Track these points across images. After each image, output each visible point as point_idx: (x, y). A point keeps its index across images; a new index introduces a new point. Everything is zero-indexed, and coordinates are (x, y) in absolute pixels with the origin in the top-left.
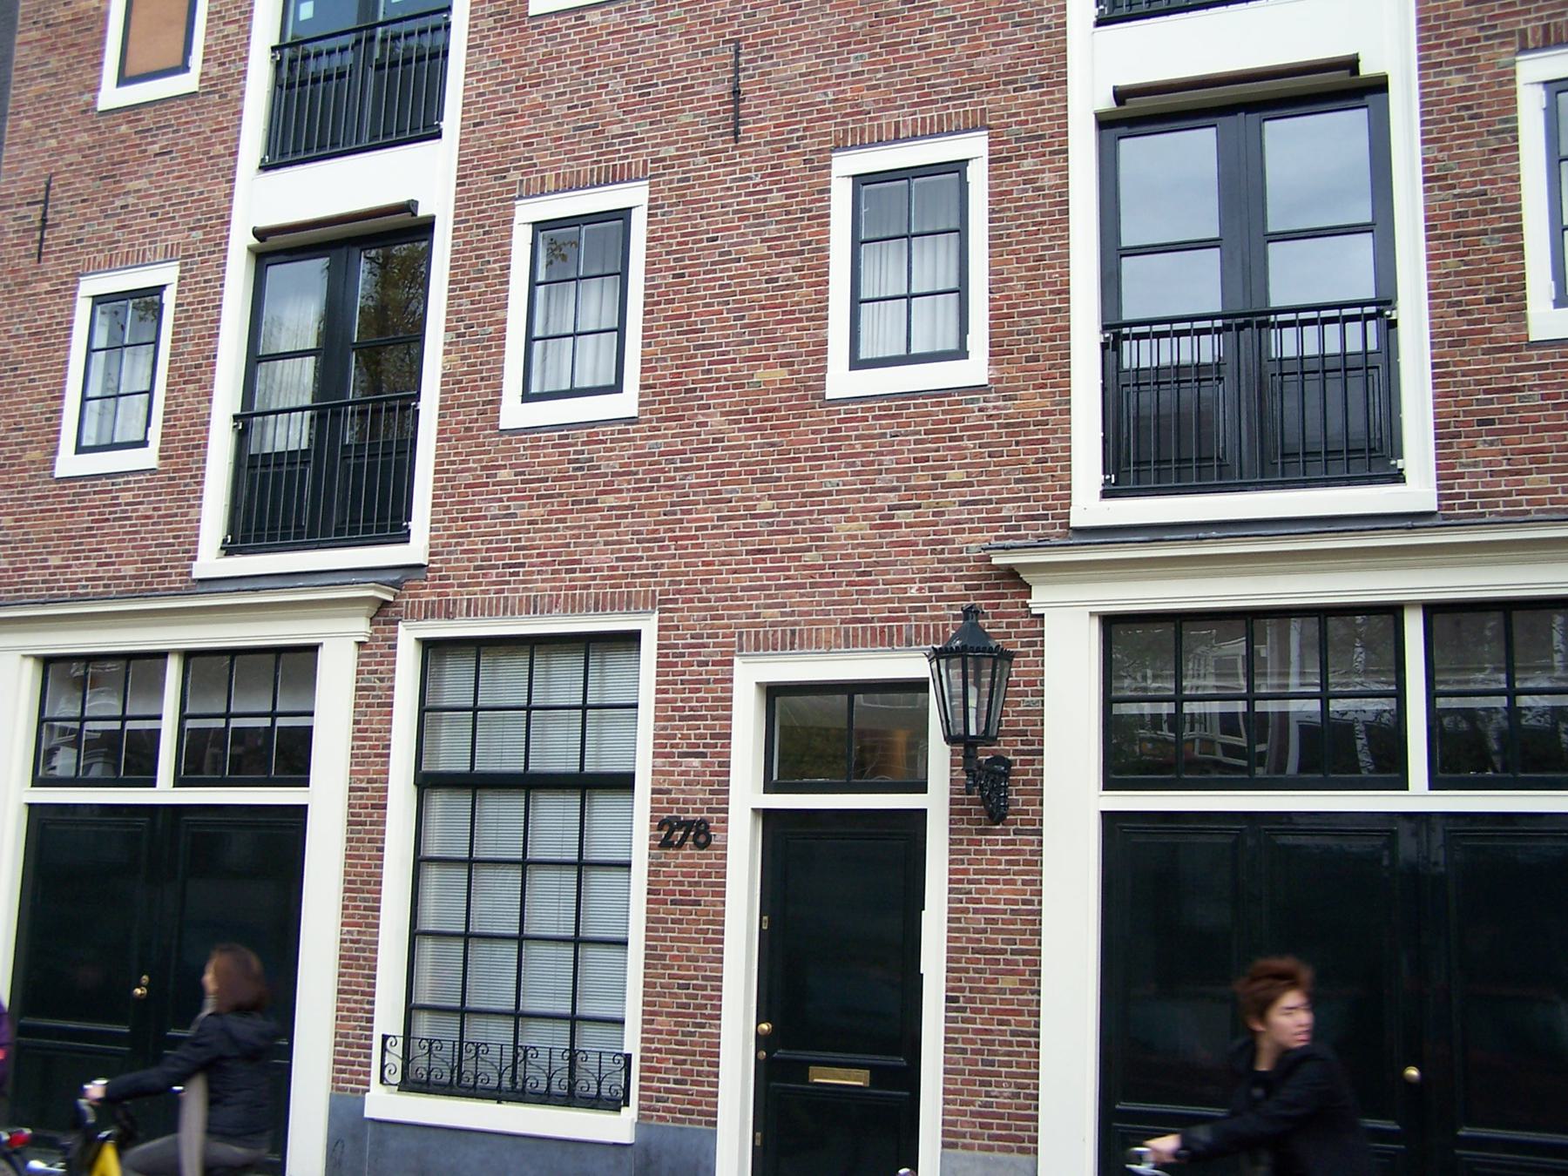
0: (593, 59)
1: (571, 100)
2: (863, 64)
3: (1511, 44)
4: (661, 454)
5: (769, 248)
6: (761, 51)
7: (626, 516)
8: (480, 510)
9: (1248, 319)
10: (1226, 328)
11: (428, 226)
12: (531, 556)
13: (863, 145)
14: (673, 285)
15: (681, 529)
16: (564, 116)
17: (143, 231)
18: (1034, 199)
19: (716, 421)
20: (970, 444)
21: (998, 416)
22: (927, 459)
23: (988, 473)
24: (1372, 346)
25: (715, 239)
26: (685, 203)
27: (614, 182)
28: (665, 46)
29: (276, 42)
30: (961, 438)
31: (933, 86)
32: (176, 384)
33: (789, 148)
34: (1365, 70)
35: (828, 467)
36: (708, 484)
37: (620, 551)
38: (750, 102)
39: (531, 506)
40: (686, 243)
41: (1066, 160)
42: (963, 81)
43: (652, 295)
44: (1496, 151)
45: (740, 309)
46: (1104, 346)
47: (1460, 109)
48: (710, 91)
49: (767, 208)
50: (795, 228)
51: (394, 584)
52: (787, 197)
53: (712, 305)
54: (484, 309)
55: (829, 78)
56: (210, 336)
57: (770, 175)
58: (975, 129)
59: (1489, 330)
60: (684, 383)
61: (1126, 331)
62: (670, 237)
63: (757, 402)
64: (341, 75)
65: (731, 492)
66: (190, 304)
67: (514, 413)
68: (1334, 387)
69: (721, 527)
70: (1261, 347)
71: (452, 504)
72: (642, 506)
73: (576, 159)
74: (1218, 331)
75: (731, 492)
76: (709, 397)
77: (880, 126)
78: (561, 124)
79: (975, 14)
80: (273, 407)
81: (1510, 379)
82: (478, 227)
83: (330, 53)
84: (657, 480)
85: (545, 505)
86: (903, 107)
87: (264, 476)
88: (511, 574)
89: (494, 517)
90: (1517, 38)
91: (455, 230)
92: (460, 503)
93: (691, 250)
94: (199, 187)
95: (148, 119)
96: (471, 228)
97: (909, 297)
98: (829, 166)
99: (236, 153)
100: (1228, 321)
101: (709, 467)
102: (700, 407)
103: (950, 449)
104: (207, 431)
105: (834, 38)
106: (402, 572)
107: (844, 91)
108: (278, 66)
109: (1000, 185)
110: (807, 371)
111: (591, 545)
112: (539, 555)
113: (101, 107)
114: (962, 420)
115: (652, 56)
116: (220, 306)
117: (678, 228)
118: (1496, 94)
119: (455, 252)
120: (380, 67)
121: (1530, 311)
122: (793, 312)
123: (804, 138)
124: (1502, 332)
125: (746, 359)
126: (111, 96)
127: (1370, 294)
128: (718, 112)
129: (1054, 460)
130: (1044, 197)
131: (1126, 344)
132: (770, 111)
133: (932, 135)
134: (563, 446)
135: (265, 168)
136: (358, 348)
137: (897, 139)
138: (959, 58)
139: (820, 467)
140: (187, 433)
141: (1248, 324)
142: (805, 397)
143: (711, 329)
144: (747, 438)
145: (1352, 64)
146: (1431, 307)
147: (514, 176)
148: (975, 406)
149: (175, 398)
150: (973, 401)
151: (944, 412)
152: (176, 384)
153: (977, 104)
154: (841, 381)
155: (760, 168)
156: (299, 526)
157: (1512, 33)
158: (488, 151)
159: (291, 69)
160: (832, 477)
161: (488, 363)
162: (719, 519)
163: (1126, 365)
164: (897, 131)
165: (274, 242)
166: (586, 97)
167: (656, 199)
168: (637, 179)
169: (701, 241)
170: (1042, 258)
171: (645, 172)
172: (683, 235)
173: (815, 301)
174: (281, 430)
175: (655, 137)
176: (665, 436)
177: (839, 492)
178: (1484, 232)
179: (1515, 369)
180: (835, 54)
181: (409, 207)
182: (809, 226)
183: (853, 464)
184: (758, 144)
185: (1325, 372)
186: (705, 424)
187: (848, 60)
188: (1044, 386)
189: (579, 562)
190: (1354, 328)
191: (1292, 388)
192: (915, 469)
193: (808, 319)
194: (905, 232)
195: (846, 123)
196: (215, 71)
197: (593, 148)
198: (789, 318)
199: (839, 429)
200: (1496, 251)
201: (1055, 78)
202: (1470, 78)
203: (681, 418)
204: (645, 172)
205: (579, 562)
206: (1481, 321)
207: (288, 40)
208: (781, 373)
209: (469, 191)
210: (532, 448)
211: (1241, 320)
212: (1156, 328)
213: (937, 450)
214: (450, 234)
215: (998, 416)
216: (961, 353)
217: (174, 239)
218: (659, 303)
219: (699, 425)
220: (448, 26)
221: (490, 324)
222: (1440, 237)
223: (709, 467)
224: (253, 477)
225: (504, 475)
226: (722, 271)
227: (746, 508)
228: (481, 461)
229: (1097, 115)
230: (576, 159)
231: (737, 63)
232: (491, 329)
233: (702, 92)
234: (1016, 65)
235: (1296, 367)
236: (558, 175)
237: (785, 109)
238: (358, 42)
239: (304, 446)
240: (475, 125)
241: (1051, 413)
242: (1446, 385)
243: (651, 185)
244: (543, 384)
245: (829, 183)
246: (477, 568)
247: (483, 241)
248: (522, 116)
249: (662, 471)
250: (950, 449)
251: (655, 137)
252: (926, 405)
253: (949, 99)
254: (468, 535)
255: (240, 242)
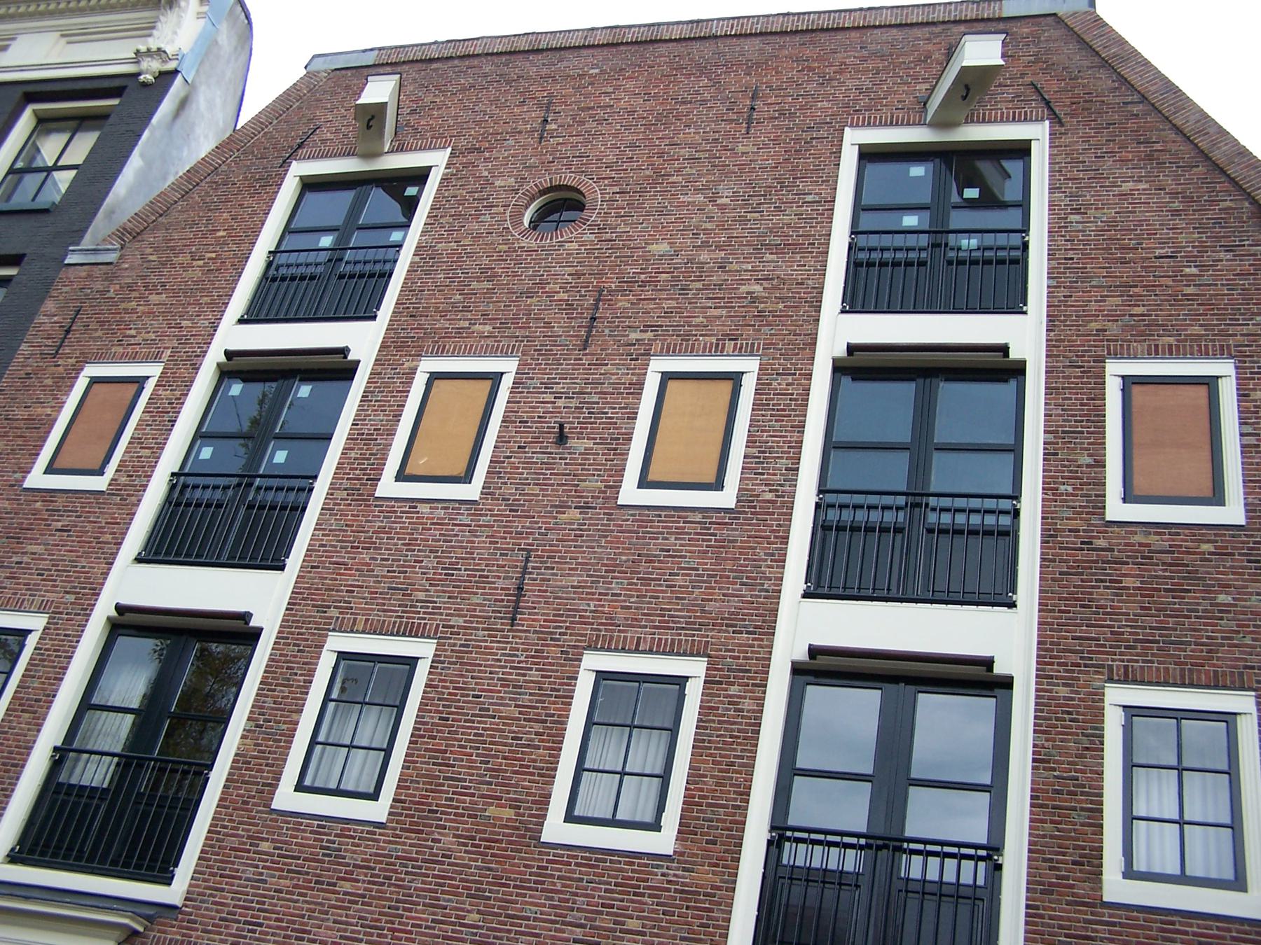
0: (416, 539)
1: (392, 566)
2: (621, 589)
3: (1102, 674)
4: (398, 858)
5: (520, 713)
6: (546, 562)
7: (356, 903)
8: (237, 871)
9: (886, 842)
10: (868, 846)
11: (256, 634)
12: (270, 919)
13: (609, 650)
14: (438, 725)
15: (400, 923)
16: (383, 576)
17: (28, 584)
18: (734, 717)
19: (448, 840)
20: (649, 900)
21: (676, 883)
22: (612, 906)
23: (660, 928)
24: (980, 882)
25: (479, 697)
26: (461, 664)
27: (410, 636)
28: (473, 542)
29: (176, 470)
30: (643, 895)
31: (673, 616)
32: (15, 710)
33: (552, 639)
34: (998, 669)
35: (531, 896)
36: (430, 891)
37: (345, 930)
38: (529, 598)
39: (280, 877)
40: (456, 695)
41: (764, 692)
42: (695, 617)
43: (419, 729)
44: (1087, 749)
45: (487, 756)
46: (770, 843)
47: (1063, 712)
48: (500, 583)
49: (525, 681)
50: (544, 702)
51: (149, 918)
52: (543, 676)
53: (465, 747)
54: (283, 710)
55: (593, 594)
56: (55, 679)
57: (533, 657)
58: (698, 655)
59: (1072, 886)
60: (430, 805)
61: (789, 834)
62: (443, 687)
63: (484, 832)
64: (219, 506)
65: (449, 900)
66: (46, 650)
67: (286, 798)
68: (947, 909)
69: (434, 928)
70: (893, 866)
71: (216, 861)
72: (371, 897)
73: (385, 611)
74: (861, 847)
75: (449, 900)
76: (446, 820)
77: (625, 638)
78: (379, 582)
79: (713, 570)
80: (89, 747)
81: (1086, 929)
82: (295, 645)
83: (205, 487)
84: (390, 878)
85: (292, 879)
86: (646, 627)
87: (64, 803)
88: (249, 931)
89: (247, 879)
90: (1106, 671)
91: (275, 643)
92: (222, 861)
93: (459, 701)
94: (84, 562)
95: (60, 502)
96: (289, 644)
97: (623, 774)
98: (580, 660)
99: (121, 544)
100: (871, 841)
101: (434, 876)
102: (438, 826)
103: (633, 901)
104: (28, 755)
105: (604, 565)
106: (159, 909)
107: (603, 606)
108: (172, 487)
109: (709, 702)
110: (531, 816)
111: (323, 920)
112: (277, 920)
113: (26, 485)
114: (647, 880)
115: (461, 547)
116: (71, 657)
117: (451, 682)
118: (1090, 707)
119: (270, 660)
120: (251, 507)
121: (1105, 877)
122: (528, 767)
123: (565, 634)
124: (1082, 889)
125: (483, 796)
126: (37, 478)
127: (983, 840)
128: (503, 600)
129: (714, 927)
130: (743, 717)
131: (787, 844)
132: (543, 608)
133: (664, 653)
134: (320, 833)
135: (139, 560)
136: (173, 716)
137: (637, 651)
138: (696, 599)
139: (524, 896)
140: (11, 753)
141: (886, 847)
142: (524, 836)
143: (462, 767)
144: (470, 859)
145: (988, 663)
146: (1029, 859)
147: (333, 613)
148: (659, 871)
149: (10, 721)
150: (658, 867)
151: (633, 871)
152: (15, 710)
153: (703, 636)
154: (555, 829)
155: (527, 650)
156: (81, 851)
157: (1103, 666)
158: (317, 589)
159: (182, 493)
160: (533, 906)
161: (275, 753)
162: (433, 921)
163: (785, 861)
164: (638, 644)
165: (129, 618)
166: (403, 566)
167: (439, 656)
168: (429, 637)
169: (468, 695)
170: (733, 764)
171: (436, 633)
172: (455, 688)
173: (547, 762)
174: (91, 767)
175: (450, 609)
176: (404, 844)
177: (535, 919)
178: (1074, 809)
179: (1090, 922)
180: (602, 577)
181: (245, 617)
182: (554, 703)
183: (552, 899)
184: (528, 631)
185: (941, 895)
186: (439, 841)
187: (611, 583)
188: (717, 865)
189: (309, 932)
190: (968, 865)
191: (913, 903)
192: (601, 913)
193: (539, 775)
194: (629, 722)
195: (600, 630)
196: (123, 480)
197: (400, 606)
198: (524, 770)
199: (547, 868)
200: (1082, 825)
201: (766, 627)
202: (1072, 692)
203: (420, 832)
204: (436, 633)
205: (309, 932)
206: (1067, 878)
207: (186, 471)
208: (508, 813)
209: (295, 615)
210: (293, 829)
211: (880, 842)
212: (813, 836)
213: (622, 901)
214: (271, 645)
215: (676, 883)
216: (655, 826)
217: (51, 596)
218: (423, 736)
219: (433, 840)
220: (311, 490)
221: (285, 723)
222: (1041, 806)
223: (434, 876)
224: (54, 802)
225: (265, 846)
226: (479, 722)
227: (457, 917)
228: (249, 830)
229: (793, 663)
230: (385, 611)
231: (525, 567)
232: (285, 727)
233: (494, 583)
234: (738, 614)
235: (918, 887)
236: (367, 620)
237: (555, 609)
238: (239, 485)
239: (105, 786)
240: (313, 567)
241: (719, 888)
242: (1035, 924)
243: (438, 644)
244: (314, 780)
245: (578, 672)
246: (221, 919)
247: (295, 656)
248: (350, 569)
249: (396, 872)
250: (633, 901)
251: (450, 609)
252: (620, 862)
253: (683, 628)
254: (222, 890)
255: (103, 610)
